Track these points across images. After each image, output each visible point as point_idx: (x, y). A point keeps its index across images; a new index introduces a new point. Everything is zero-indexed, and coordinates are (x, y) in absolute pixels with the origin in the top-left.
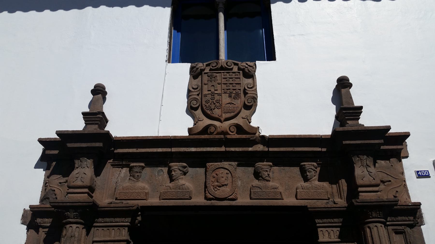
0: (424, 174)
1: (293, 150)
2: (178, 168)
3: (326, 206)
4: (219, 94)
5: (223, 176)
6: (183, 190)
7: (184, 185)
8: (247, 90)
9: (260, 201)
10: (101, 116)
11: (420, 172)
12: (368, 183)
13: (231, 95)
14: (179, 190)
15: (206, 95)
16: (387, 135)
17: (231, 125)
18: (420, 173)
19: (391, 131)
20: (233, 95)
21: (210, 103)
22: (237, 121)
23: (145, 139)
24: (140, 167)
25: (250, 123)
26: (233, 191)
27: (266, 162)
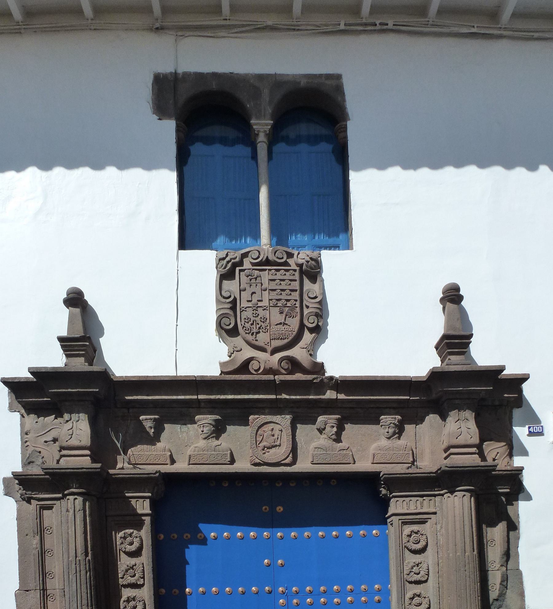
0: (537, 431)
4: (265, 308)
5: (273, 434)
11: (532, 428)
13: (284, 309)
15: (243, 309)
16: (499, 377)
18: (531, 429)
19: (504, 373)
22: (297, 352)
23: (158, 380)
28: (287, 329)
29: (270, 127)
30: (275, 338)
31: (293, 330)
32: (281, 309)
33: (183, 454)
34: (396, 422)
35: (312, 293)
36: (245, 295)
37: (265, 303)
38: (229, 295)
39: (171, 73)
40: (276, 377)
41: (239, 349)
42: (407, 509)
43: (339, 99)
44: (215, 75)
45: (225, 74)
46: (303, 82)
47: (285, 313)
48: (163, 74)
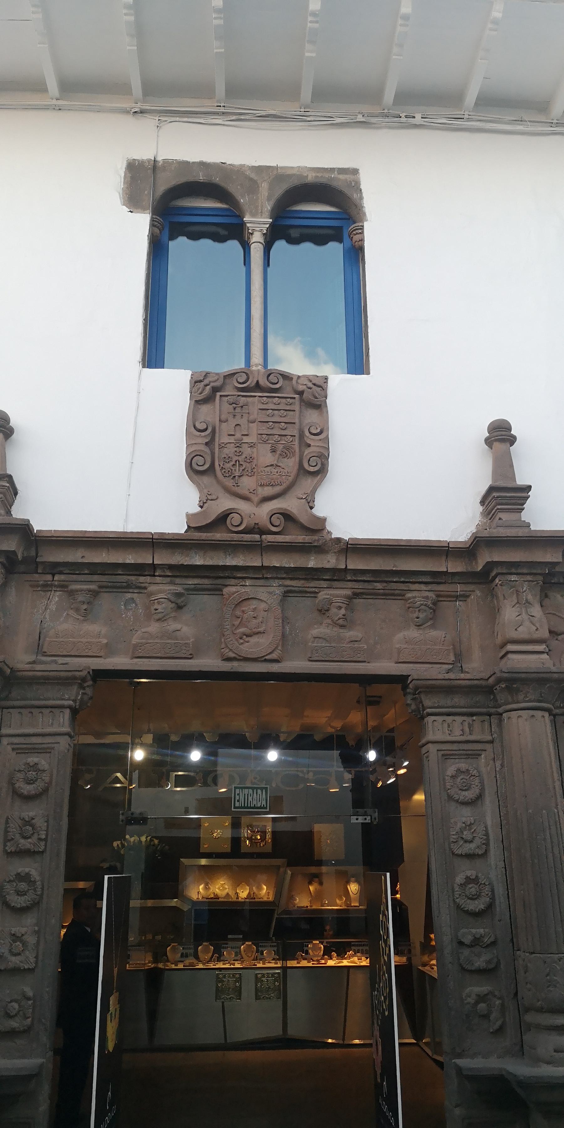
1: (394, 569)
4: (252, 444)
5: (255, 615)
6: (177, 640)
7: (180, 630)
8: (308, 437)
9: (325, 665)
10: (8, 485)
12: (525, 636)
13: (276, 447)
14: (169, 641)
15: (223, 445)
17: (276, 512)
20: (280, 447)
21: (232, 463)
24: (90, 593)
25: (311, 508)
28: (280, 472)
29: (268, 226)
30: (264, 484)
31: (289, 475)
32: (273, 447)
33: (125, 642)
34: (429, 603)
35: (315, 428)
36: (226, 428)
37: (252, 439)
38: (205, 427)
39: (149, 161)
40: (264, 537)
41: (214, 497)
42: (450, 734)
43: (355, 196)
44: (202, 164)
45: (214, 163)
46: (311, 178)
47: (278, 452)
48: (138, 161)
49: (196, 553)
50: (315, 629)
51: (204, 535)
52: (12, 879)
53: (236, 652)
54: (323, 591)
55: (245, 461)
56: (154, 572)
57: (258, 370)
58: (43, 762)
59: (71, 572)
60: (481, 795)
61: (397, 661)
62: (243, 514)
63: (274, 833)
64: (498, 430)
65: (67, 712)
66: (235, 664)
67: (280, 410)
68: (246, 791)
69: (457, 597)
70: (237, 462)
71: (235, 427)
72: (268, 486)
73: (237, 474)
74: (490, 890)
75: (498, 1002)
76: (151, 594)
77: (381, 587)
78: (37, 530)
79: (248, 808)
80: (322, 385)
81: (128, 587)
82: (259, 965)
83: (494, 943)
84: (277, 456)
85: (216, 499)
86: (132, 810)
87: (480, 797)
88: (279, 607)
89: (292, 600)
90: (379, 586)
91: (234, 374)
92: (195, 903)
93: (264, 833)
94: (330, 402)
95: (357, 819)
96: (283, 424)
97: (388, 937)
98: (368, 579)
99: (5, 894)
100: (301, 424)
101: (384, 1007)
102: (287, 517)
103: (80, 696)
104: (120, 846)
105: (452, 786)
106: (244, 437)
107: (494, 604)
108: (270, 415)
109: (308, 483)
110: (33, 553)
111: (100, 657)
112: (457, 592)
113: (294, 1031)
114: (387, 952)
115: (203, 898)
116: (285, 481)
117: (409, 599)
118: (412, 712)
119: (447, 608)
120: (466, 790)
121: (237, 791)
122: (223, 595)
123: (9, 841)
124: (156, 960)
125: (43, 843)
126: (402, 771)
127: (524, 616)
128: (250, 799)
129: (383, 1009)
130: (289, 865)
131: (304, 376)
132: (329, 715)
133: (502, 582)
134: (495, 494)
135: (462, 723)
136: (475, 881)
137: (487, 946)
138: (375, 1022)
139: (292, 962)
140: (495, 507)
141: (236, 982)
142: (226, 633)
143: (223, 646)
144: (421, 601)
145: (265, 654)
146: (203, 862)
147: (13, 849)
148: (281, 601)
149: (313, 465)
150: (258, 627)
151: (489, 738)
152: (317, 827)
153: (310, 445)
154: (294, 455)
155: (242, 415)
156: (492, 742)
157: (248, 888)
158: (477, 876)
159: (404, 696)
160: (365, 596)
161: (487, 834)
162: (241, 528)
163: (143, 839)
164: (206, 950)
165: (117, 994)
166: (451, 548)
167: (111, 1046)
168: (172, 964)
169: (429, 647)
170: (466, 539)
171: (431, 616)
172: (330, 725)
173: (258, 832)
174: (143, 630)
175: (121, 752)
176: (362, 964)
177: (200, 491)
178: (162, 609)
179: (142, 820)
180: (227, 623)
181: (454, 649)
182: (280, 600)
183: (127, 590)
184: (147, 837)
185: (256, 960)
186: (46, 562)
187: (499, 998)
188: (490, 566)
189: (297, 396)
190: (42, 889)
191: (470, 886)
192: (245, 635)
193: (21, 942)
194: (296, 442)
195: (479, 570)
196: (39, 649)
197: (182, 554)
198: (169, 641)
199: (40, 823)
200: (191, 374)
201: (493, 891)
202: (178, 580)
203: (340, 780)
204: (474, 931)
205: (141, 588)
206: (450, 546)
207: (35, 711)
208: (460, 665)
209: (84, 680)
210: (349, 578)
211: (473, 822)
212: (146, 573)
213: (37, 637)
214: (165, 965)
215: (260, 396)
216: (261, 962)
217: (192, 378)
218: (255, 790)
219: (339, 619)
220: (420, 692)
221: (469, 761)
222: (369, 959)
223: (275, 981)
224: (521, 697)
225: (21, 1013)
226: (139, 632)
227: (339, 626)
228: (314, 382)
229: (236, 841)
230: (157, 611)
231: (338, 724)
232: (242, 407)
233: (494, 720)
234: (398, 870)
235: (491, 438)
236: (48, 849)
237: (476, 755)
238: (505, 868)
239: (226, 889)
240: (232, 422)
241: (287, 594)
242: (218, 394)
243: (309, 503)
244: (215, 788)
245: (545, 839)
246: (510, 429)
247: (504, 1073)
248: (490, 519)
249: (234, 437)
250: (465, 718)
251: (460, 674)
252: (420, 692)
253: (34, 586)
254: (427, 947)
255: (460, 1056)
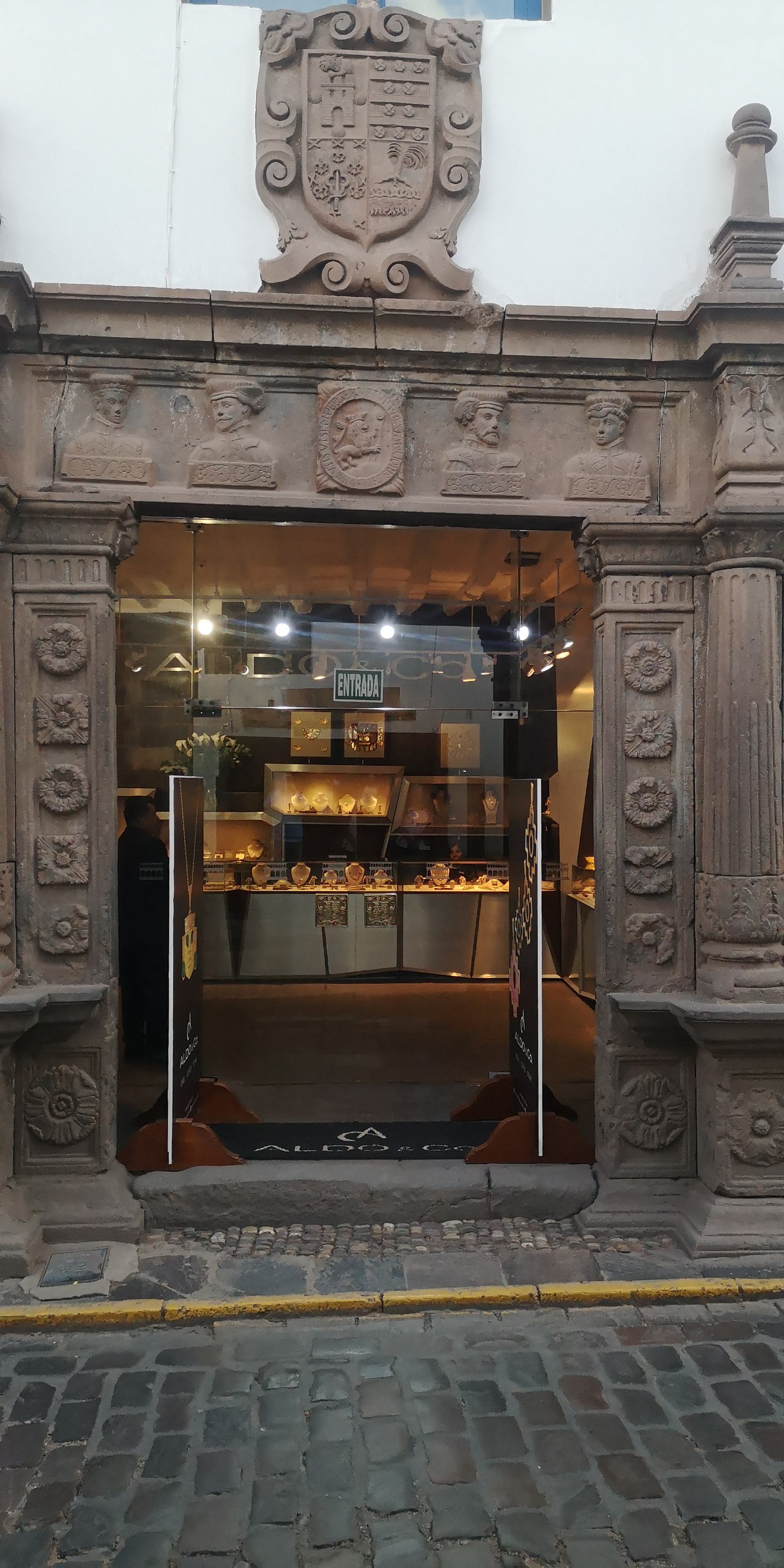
2: (234, 395)
3: (637, 521)
4: (359, 143)
6: (253, 460)
8: (448, 132)
13: (399, 148)
14: (242, 463)
15: (314, 143)
20: (404, 148)
25: (451, 254)
26: (395, 472)
27: (286, 843)
32: (393, 147)
34: (620, 411)
35: (461, 116)
38: (285, 111)
40: (378, 301)
41: (301, 234)
49: (276, 326)
50: (453, 448)
51: (288, 297)
52: (49, 777)
53: (338, 480)
54: (465, 390)
55: (349, 172)
56: (215, 356)
57: (370, 9)
58: (77, 630)
59: (92, 352)
60: (670, 682)
61: (567, 496)
62: (345, 263)
63: (388, 735)
64: (751, 122)
65: (103, 561)
66: (337, 498)
67: (405, 82)
68: (352, 676)
69: (662, 400)
70: (337, 173)
71: (332, 112)
72: (384, 215)
73: (337, 194)
74: (671, 800)
75: (669, 931)
76: (211, 391)
77: (551, 385)
78: (36, 284)
79: (354, 698)
80: (473, 38)
81: (176, 379)
82: (367, 890)
83: (670, 864)
84: (399, 163)
85: (306, 237)
86: (200, 698)
87: (668, 685)
88: (400, 415)
89: (421, 404)
90: (548, 382)
91: (329, 16)
92: (286, 817)
93: (374, 735)
94: (485, 68)
95: (500, 715)
96: (409, 107)
97: (535, 854)
98: (534, 372)
99: (41, 795)
100: (437, 107)
101: (526, 935)
102: (414, 269)
103: (119, 540)
104: (185, 746)
105: (632, 670)
106: (348, 130)
107: (716, 412)
108: (389, 91)
109: (446, 210)
110: (33, 320)
111: (144, 483)
112: (662, 393)
113: (411, 962)
114: (533, 872)
115: (296, 811)
116: (412, 207)
117: (592, 403)
118: (584, 571)
119: (646, 416)
120: (651, 676)
121: (341, 676)
122: (317, 394)
123: (41, 729)
124: (238, 882)
125: (86, 733)
126: (562, 655)
127: (759, 430)
128: (358, 686)
129: (525, 938)
130: (407, 773)
131: (444, 21)
132: (465, 580)
133: (732, 377)
134: (736, 234)
135: (653, 586)
136: (653, 789)
137: (662, 867)
138: (514, 951)
139: (409, 886)
140: (733, 254)
141: (342, 904)
142: (323, 453)
143: (319, 471)
144: (608, 406)
145: (380, 484)
146: (295, 768)
147: (47, 741)
148: (403, 405)
149: (456, 181)
150: (369, 445)
151: (689, 606)
152: (445, 728)
153: (452, 145)
154: (426, 163)
155: (344, 91)
156: (692, 612)
157: (354, 801)
158: (655, 784)
159: (575, 547)
160: (526, 400)
161: (674, 733)
162: (343, 287)
163: (215, 738)
164: (300, 871)
165: (194, 915)
166: (660, 322)
167: (188, 972)
168: (260, 886)
169: (614, 476)
170: (684, 309)
171: (621, 431)
172: (465, 593)
173: (366, 733)
174: (204, 445)
175: (179, 622)
176: (497, 890)
177: (280, 222)
178: (230, 414)
179: (213, 711)
180: (325, 437)
181: (651, 479)
182: (401, 403)
183: (176, 384)
184: (220, 737)
185: (365, 883)
186: (55, 335)
187: (671, 926)
188: (717, 350)
189: (432, 58)
190: (90, 788)
191: (647, 795)
192: (350, 455)
193: (67, 852)
194: (430, 141)
195: (698, 359)
196: (55, 468)
197: (256, 327)
198: (242, 463)
199: (80, 708)
200: (260, 15)
201: (674, 801)
202: (251, 370)
203: (477, 669)
204: (645, 848)
205: (196, 381)
206: (659, 319)
207: (60, 559)
208: (657, 503)
209: (123, 516)
210: (504, 370)
211: (655, 717)
212: (204, 357)
213: (52, 453)
214: (250, 888)
215: (373, 57)
216: (371, 886)
217: (262, 22)
218: (364, 676)
219: (488, 433)
220: (598, 542)
221: (659, 637)
222: (508, 883)
223: (389, 905)
224: (740, 549)
225: (75, 933)
226: (198, 448)
227: (488, 444)
228: (460, 32)
229: (338, 745)
230: (222, 417)
231: (477, 592)
232: (343, 76)
233: (698, 582)
234: (548, 781)
235: (737, 138)
236: (93, 741)
237: (668, 629)
238: (694, 773)
239: (326, 801)
240: (329, 102)
241: (411, 394)
242: (306, 52)
243: (447, 245)
244: (308, 675)
245: (750, 739)
246: (767, 121)
247: (669, 1008)
248: (723, 276)
249: (330, 129)
250: (657, 579)
251: (656, 516)
252: (598, 542)
253: (39, 373)
254: (580, 872)
255: (616, 989)
